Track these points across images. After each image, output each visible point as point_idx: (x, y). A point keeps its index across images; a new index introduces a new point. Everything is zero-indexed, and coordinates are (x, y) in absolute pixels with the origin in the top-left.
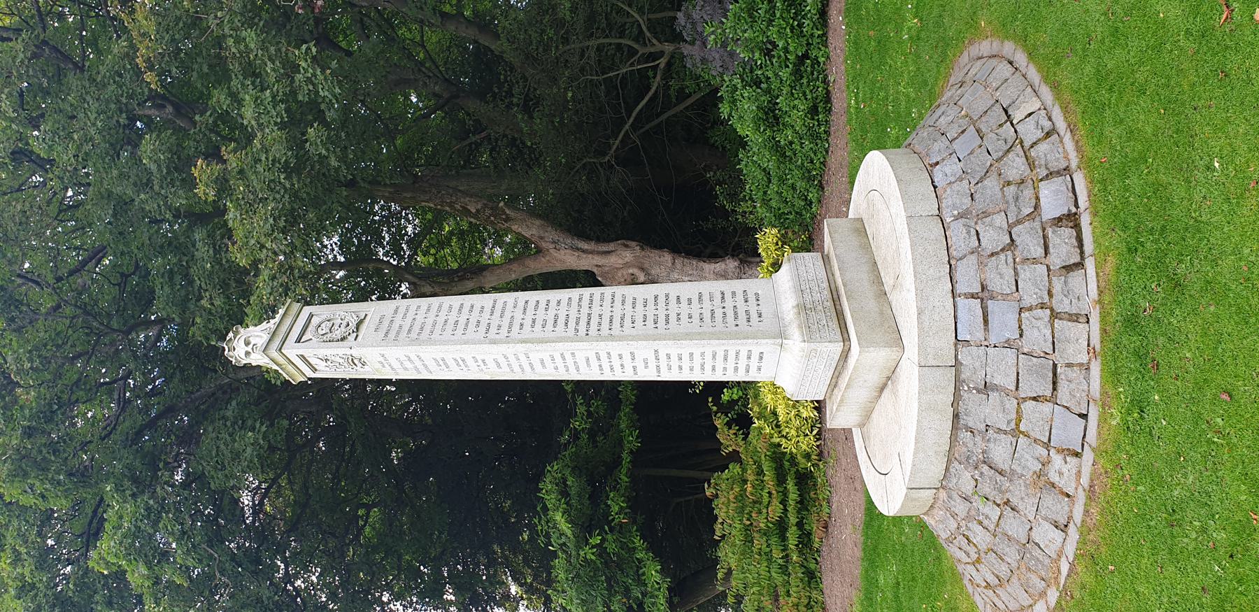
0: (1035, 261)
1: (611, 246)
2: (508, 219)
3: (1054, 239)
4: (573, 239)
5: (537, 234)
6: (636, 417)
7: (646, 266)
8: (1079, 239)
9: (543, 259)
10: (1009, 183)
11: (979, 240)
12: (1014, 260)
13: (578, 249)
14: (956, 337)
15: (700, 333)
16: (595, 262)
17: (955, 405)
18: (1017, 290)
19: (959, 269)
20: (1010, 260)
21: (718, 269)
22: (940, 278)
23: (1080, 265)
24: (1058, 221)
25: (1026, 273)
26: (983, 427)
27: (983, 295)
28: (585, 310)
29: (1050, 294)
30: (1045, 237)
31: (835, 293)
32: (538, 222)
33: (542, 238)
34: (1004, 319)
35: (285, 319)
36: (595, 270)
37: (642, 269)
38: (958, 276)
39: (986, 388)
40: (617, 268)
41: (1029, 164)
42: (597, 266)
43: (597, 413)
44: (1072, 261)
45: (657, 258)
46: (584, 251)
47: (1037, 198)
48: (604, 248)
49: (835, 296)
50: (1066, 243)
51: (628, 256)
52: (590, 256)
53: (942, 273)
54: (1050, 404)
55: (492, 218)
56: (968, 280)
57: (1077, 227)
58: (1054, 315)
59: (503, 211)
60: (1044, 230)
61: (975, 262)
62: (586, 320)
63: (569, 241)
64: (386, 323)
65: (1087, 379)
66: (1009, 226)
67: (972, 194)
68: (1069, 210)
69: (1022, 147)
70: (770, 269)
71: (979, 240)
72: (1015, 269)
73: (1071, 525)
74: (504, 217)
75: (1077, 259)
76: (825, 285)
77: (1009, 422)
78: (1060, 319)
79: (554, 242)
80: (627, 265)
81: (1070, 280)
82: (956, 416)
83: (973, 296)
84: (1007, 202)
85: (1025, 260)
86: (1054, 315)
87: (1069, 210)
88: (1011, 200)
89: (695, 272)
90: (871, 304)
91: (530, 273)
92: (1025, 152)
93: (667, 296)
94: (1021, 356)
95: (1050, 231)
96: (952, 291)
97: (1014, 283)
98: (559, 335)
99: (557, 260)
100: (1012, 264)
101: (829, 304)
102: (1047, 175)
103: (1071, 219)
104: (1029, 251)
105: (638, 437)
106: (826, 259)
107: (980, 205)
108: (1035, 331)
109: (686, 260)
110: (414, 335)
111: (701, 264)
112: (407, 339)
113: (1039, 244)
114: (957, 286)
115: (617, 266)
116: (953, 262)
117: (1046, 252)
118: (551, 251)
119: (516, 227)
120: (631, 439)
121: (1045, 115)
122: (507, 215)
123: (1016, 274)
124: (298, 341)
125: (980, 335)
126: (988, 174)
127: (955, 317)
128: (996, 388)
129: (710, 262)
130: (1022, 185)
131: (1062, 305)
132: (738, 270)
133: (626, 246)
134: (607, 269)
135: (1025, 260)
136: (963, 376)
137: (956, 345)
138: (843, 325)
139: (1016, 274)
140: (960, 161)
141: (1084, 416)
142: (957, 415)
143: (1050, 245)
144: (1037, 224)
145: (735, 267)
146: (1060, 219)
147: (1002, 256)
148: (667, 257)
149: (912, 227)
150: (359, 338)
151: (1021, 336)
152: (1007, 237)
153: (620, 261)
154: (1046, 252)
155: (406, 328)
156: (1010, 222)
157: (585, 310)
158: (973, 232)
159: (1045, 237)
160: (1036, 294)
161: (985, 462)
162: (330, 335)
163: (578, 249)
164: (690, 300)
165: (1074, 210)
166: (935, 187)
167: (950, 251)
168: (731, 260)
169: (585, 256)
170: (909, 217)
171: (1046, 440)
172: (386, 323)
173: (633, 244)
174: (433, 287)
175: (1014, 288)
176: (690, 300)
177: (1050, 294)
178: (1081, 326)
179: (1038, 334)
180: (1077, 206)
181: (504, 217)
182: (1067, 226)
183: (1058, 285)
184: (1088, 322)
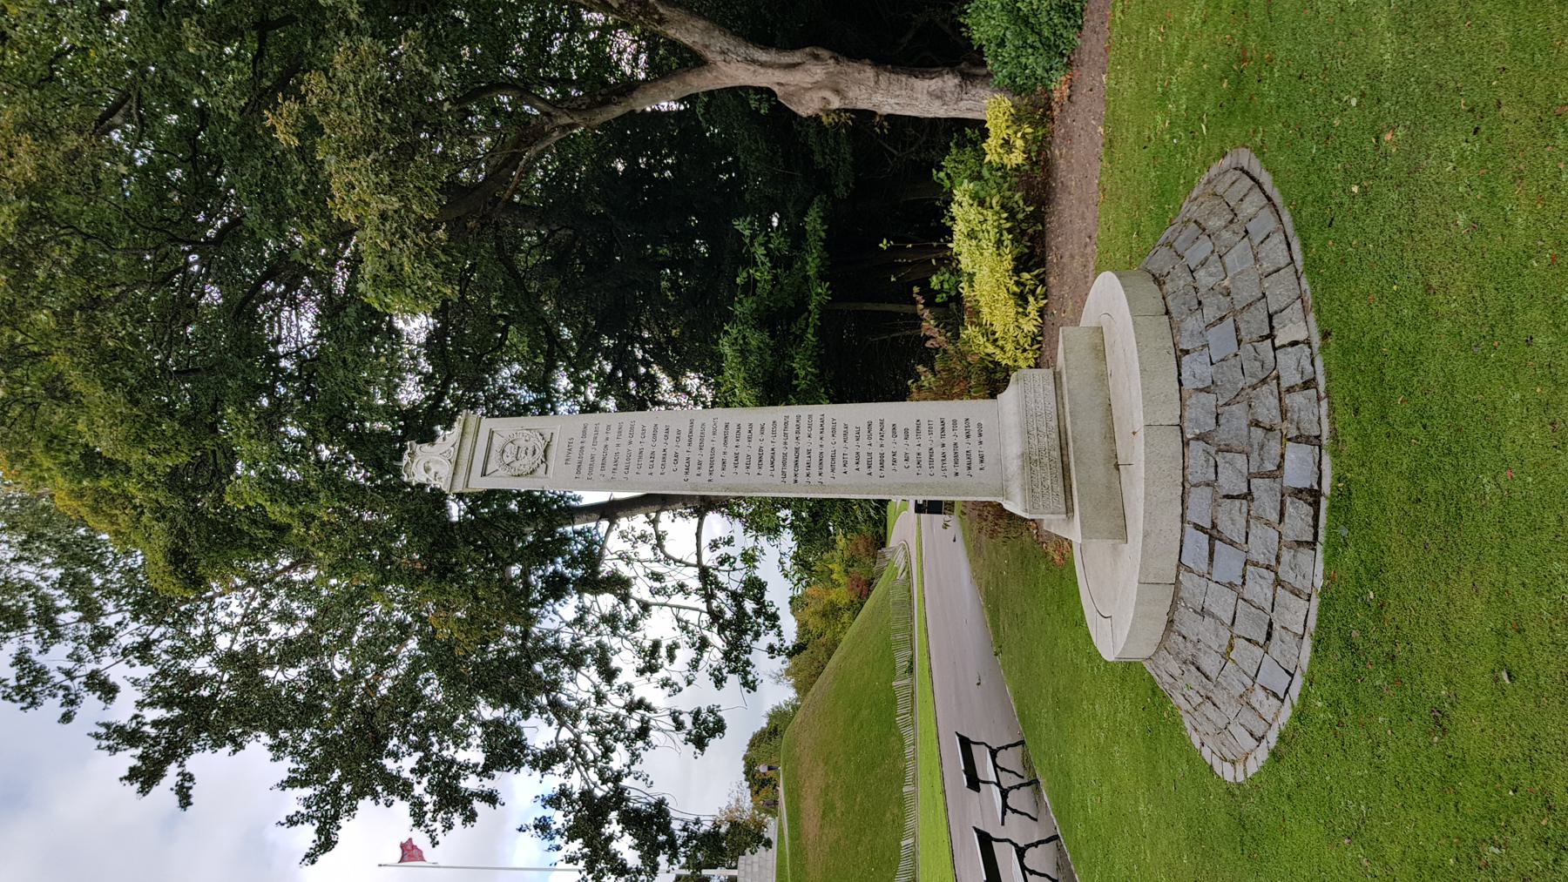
0: (1268, 524)
1: (796, 57)
2: (661, 21)
3: (1290, 509)
4: (747, 47)
5: (701, 42)
6: (826, 255)
7: (842, 86)
8: (1316, 518)
9: (709, 75)
10: (1257, 424)
11: (1216, 473)
12: (1249, 511)
13: (754, 61)
14: (1180, 560)
15: (917, 485)
16: (776, 80)
17: (1171, 614)
18: (1247, 543)
19: (1192, 495)
20: (1244, 509)
21: (933, 87)
22: (1171, 501)
23: (1312, 545)
24: (1298, 493)
25: (1257, 530)
26: (1195, 640)
27: (1213, 534)
28: (792, 443)
29: (1278, 558)
30: (1282, 503)
31: (1063, 436)
32: (701, 24)
33: (707, 47)
34: (1229, 563)
35: (465, 441)
36: (776, 89)
37: (837, 92)
38: (1190, 501)
39: (1203, 612)
40: (804, 88)
41: (1281, 411)
42: (778, 84)
43: (779, 251)
44: (1304, 539)
45: (856, 75)
46: (762, 65)
47: (1282, 456)
48: (787, 58)
49: (1063, 442)
50: (1302, 519)
51: (817, 72)
52: (770, 71)
53: (1174, 496)
54: (1262, 651)
55: (641, 18)
56: (1200, 510)
57: (1316, 505)
58: (1278, 582)
59: (655, 8)
60: (1283, 495)
61: (1210, 496)
62: (794, 459)
63: (742, 50)
64: (576, 451)
65: (1300, 648)
66: (1249, 474)
67: (1218, 415)
68: (1312, 486)
69: (1279, 384)
70: (999, 150)
71: (1216, 473)
72: (1248, 521)
73: (1264, 741)
74: (656, 17)
75: (1310, 539)
76: (1054, 424)
77: (1220, 646)
78: (1283, 587)
79: (723, 52)
80: (817, 86)
81: (1299, 555)
82: (1171, 622)
83: (1202, 529)
84: (1252, 446)
85: (1259, 518)
86: (1278, 582)
87: (1312, 486)
88: (1256, 446)
89: (904, 92)
90: (1100, 473)
91: (694, 91)
92: (1280, 393)
93: (882, 423)
94: (1240, 600)
95: (1288, 500)
96: (1182, 515)
97: (1244, 534)
98: (765, 481)
99: (727, 77)
100: (1245, 515)
101: (1056, 454)
102: (1297, 437)
103: (1313, 496)
104: (1264, 510)
105: (828, 289)
106: (1057, 377)
107: (1222, 436)
108: (1258, 588)
109: (893, 76)
110: (608, 472)
111: (913, 80)
112: (602, 479)
113: (1275, 509)
114: (1188, 512)
115: (805, 85)
116: (1187, 486)
117: (1281, 520)
118: (718, 63)
119: (673, 31)
120: (820, 291)
121: (1308, 354)
122: (661, 15)
123: (1248, 526)
124: (484, 474)
125: (1204, 567)
126: (1238, 399)
127: (1182, 541)
128: (1212, 615)
129: (924, 78)
130: (1270, 433)
131: (1287, 574)
132: (958, 89)
133: (816, 57)
134: (792, 88)
135: (1259, 518)
136: (1181, 594)
137: (1178, 567)
138: (1068, 489)
139: (1248, 526)
140: (1212, 364)
141: (1292, 676)
142: (1172, 621)
143: (1286, 515)
144: (1277, 486)
145: (955, 86)
146: (1300, 491)
147: (1237, 502)
148: (869, 72)
149: (1148, 439)
150: (551, 470)
151: (1244, 583)
152: (1246, 484)
153: (809, 79)
154: (1281, 520)
155: (598, 461)
156: (1251, 471)
157: (792, 443)
158: (1212, 462)
159: (1282, 503)
160: (1264, 554)
161: (1193, 664)
162: (516, 464)
163: (754, 61)
164: (906, 431)
165: (1316, 487)
166: (1181, 384)
167: (1187, 472)
168: (950, 76)
169: (762, 71)
170: (1130, 663)
171: (1253, 675)
172: (576, 451)
173: (824, 53)
174: (572, 118)
175: (1244, 540)
176: (906, 431)
177: (1278, 558)
178: (1302, 602)
179: (1260, 588)
180: (1319, 483)
181: (656, 17)
182: (1305, 501)
183: (1286, 556)
184: (1309, 600)
